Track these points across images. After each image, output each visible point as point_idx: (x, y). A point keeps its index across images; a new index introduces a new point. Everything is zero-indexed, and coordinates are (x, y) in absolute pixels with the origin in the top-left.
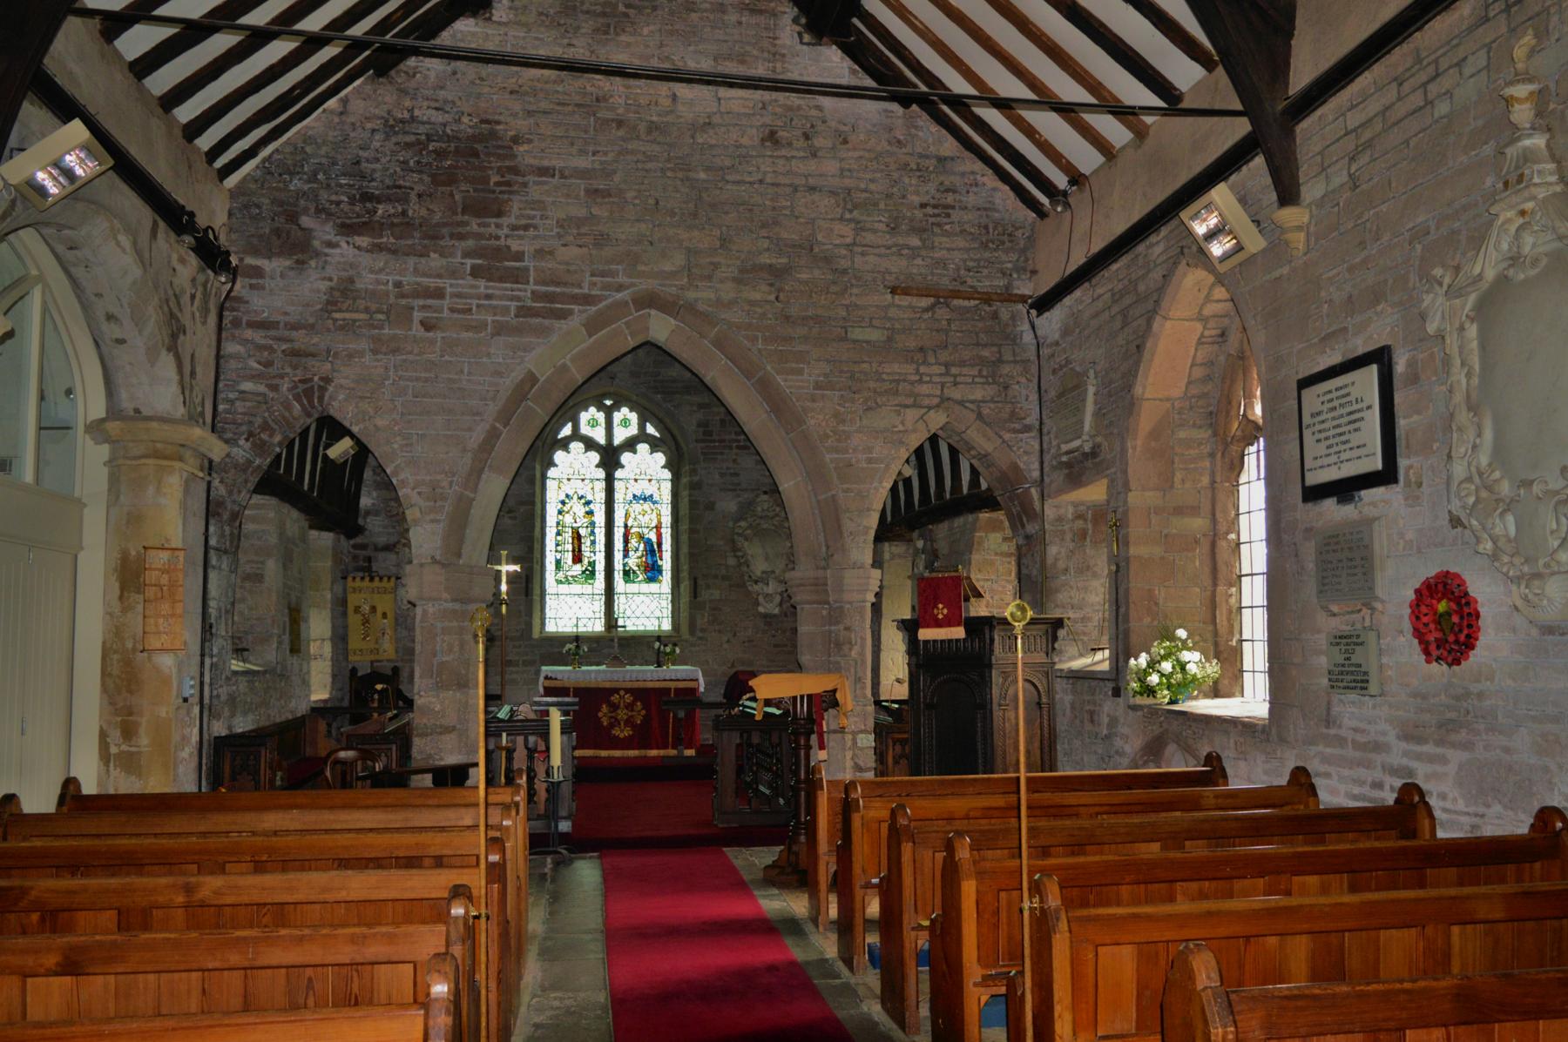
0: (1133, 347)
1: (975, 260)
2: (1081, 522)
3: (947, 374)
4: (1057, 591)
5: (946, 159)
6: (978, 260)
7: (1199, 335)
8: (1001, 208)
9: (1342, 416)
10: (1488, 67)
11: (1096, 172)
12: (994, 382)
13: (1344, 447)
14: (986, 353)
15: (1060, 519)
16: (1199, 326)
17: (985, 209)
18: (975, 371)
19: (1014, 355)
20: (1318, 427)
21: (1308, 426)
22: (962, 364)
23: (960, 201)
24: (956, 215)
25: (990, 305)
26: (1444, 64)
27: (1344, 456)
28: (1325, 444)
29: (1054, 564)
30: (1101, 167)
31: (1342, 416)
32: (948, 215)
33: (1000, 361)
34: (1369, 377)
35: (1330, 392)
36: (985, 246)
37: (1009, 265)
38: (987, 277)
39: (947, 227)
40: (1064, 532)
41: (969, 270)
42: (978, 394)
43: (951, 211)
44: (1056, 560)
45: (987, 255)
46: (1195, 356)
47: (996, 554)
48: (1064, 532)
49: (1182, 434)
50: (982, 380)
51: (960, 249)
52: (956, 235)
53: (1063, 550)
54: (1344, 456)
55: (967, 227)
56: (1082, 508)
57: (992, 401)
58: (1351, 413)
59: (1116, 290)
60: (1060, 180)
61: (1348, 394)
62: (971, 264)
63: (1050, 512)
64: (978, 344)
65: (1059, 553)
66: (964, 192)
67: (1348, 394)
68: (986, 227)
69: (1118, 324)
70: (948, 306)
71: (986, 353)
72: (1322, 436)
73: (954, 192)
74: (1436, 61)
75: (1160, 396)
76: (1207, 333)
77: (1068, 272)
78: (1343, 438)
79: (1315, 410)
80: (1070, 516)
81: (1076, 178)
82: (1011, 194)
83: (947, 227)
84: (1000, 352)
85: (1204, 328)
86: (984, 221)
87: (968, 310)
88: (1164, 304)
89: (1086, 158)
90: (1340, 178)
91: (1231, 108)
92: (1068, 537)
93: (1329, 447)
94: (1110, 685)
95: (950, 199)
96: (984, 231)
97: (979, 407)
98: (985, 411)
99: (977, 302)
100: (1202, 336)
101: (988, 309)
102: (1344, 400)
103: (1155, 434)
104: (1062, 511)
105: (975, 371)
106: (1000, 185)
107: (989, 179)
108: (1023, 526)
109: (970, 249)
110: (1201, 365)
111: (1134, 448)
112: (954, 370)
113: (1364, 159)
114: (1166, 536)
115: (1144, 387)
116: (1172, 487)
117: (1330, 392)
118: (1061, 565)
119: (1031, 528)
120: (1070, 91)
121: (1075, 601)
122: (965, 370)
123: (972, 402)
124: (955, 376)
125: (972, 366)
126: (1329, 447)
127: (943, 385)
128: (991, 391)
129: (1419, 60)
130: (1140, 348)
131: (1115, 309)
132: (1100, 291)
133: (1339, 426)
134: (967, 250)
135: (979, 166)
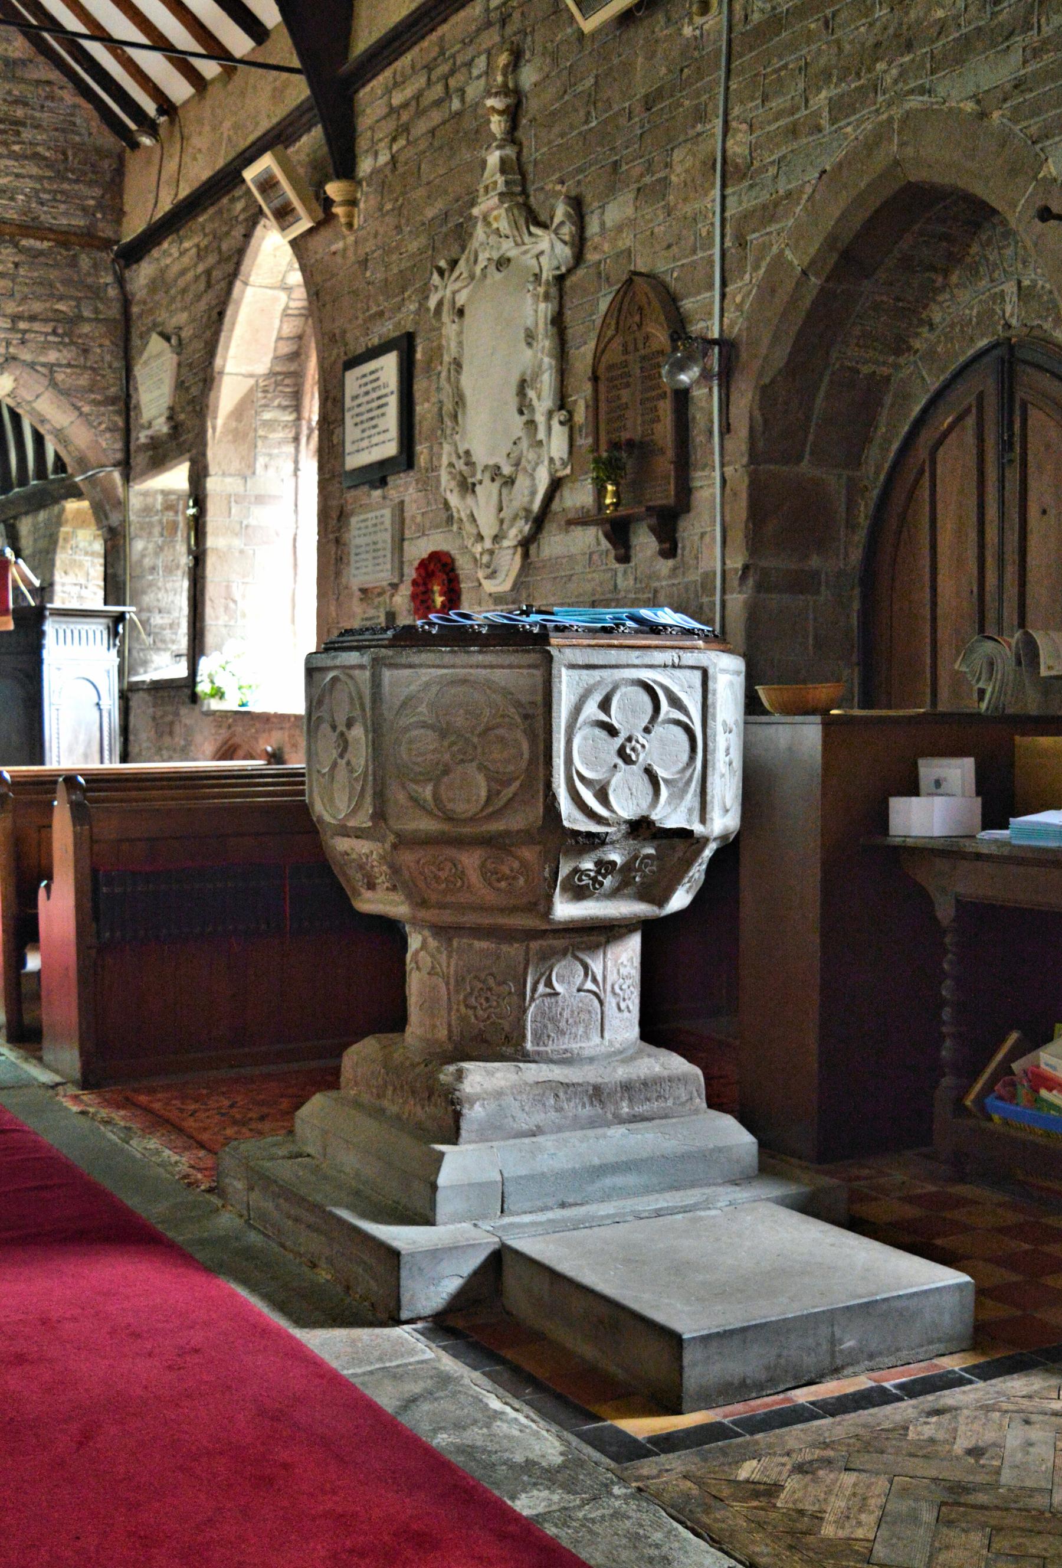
0: (214, 314)
1: (49, 192)
2: (171, 514)
3: (13, 329)
4: (144, 592)
5: (15, 62)
6: (55, 192)
7: (282, 306)
8: (83, 131)
9: (373, 401)
10: (487, 73)
11: (186, 103)
12: (72, 343)
13: (373, 431)
14: (61, 306)
15: (147, 510)
16: (283, 296)
17: (63, 131)
18: (48, 329)
19: (96, 311)
20: (357, 410)
21: (349, 409)
22: (33, 318)
23: (33, 118)
24: (27, 134)
25: (68, 250)
26: (459, 61)
27: (375, 440)
28: (361, 427)
29: (140, 562)
30: (193, 97)
31: (373, 401)
32: (18, 133)
33: (79, 318)
34: (388, 365)
35: (364, 376)
36: (61, 177)
37: (92, 202)
38: (63, 214)
39: (16, 148)
40: (151, 525)
41: (42, 204)
42: (52, 356)
43: (21, 129)
44: (143, 556)
45: (66, 186)
46: (280, 328)
47: (86, 553)
48: (151, 525)
49: (267, 416)
50: (57, 339)
51: (31, 177)
52: (26, 157)
53: (151, 546)
54: (375, 440)
55: (40, 149)
56: (173, 497)
57: (69, 365)
58: (379, 398)
59: (202, 245)
60: (150, 107)
61: (378, 379)
62: (45, 196)
63: (135, 502)
64: (52, 296)
65: (145, 549)
66: (37, 107)
67: (378, 379)
68: (64, 154)
69: (202, 285)
70: (16, 245)
71: (61, 306)
72: (358, 419)
73: (26, 104)
74: (453, 56)
75: (243, 371)
76: (292, 304)
77: (159, 214)
78: (373, 422)
79: (355, 393)
80: (159, 507)
81: (166, 106)
82: (95, 114)
83: (16, 148)
84: (78, 307)
85: (289, 298)
86: (61, 143)
87: (41, 253)
88: (244, 268)
89: (179, 89)
90: (384, 158)
91: (292, 65)
92: (156, 531)
93: (375, 427)
94: (187, 691)
95: (20, 112)
96: (61, 157)
97: (52, 372)
98: (60, 377)
99: (50, 244)
100: (287, 308)
101: (65, 253)
102: (375, 385)
103: (239, 412)
104: (150, 500)
105: (48, 329)
106: (80, 101)
107: (69, 96)
108: (107, 518)
109: (44, 177)
110: (288, 339)
111: (214, 429)
112: (22, 325)
113: (401, 142)
114: (247, 527)
115: (225, 360)
116: (254, 473)
117: (364, 376)
118: (147, 562)
119: (115, 519)
120: (97, 50)
121: (162, 605)
122: (37, 326)
123: (43, 365)
124: (24, 332)
125: (46, 320)
126: (363, 431)
127: (8, 344)
128: (66, 355)
129: (442, 52)
130: (221, 314)
131: (201, 268)
132: (186, 245)
133: (370, 410)
134: (40, 179)
135: (55, 75)
